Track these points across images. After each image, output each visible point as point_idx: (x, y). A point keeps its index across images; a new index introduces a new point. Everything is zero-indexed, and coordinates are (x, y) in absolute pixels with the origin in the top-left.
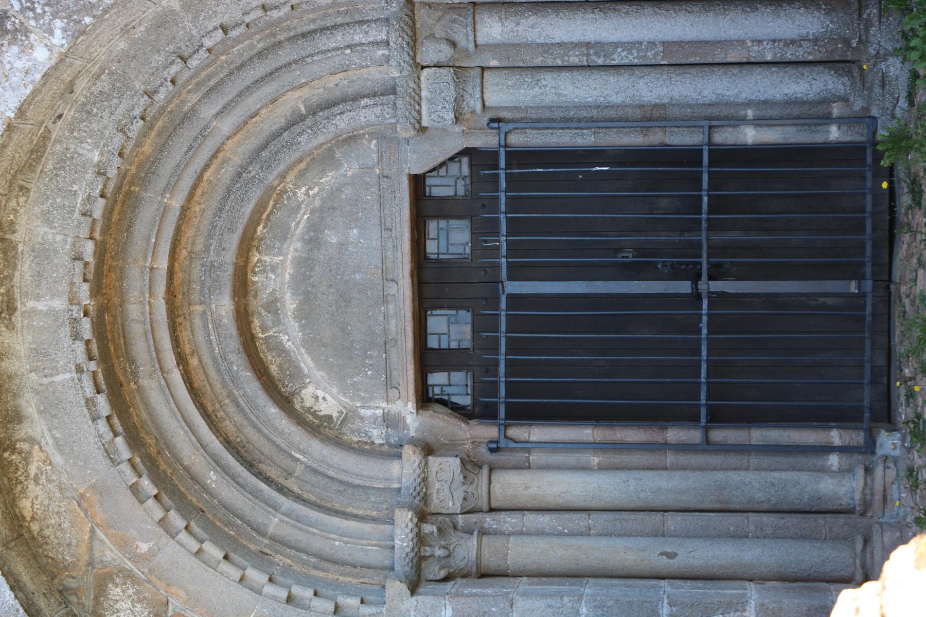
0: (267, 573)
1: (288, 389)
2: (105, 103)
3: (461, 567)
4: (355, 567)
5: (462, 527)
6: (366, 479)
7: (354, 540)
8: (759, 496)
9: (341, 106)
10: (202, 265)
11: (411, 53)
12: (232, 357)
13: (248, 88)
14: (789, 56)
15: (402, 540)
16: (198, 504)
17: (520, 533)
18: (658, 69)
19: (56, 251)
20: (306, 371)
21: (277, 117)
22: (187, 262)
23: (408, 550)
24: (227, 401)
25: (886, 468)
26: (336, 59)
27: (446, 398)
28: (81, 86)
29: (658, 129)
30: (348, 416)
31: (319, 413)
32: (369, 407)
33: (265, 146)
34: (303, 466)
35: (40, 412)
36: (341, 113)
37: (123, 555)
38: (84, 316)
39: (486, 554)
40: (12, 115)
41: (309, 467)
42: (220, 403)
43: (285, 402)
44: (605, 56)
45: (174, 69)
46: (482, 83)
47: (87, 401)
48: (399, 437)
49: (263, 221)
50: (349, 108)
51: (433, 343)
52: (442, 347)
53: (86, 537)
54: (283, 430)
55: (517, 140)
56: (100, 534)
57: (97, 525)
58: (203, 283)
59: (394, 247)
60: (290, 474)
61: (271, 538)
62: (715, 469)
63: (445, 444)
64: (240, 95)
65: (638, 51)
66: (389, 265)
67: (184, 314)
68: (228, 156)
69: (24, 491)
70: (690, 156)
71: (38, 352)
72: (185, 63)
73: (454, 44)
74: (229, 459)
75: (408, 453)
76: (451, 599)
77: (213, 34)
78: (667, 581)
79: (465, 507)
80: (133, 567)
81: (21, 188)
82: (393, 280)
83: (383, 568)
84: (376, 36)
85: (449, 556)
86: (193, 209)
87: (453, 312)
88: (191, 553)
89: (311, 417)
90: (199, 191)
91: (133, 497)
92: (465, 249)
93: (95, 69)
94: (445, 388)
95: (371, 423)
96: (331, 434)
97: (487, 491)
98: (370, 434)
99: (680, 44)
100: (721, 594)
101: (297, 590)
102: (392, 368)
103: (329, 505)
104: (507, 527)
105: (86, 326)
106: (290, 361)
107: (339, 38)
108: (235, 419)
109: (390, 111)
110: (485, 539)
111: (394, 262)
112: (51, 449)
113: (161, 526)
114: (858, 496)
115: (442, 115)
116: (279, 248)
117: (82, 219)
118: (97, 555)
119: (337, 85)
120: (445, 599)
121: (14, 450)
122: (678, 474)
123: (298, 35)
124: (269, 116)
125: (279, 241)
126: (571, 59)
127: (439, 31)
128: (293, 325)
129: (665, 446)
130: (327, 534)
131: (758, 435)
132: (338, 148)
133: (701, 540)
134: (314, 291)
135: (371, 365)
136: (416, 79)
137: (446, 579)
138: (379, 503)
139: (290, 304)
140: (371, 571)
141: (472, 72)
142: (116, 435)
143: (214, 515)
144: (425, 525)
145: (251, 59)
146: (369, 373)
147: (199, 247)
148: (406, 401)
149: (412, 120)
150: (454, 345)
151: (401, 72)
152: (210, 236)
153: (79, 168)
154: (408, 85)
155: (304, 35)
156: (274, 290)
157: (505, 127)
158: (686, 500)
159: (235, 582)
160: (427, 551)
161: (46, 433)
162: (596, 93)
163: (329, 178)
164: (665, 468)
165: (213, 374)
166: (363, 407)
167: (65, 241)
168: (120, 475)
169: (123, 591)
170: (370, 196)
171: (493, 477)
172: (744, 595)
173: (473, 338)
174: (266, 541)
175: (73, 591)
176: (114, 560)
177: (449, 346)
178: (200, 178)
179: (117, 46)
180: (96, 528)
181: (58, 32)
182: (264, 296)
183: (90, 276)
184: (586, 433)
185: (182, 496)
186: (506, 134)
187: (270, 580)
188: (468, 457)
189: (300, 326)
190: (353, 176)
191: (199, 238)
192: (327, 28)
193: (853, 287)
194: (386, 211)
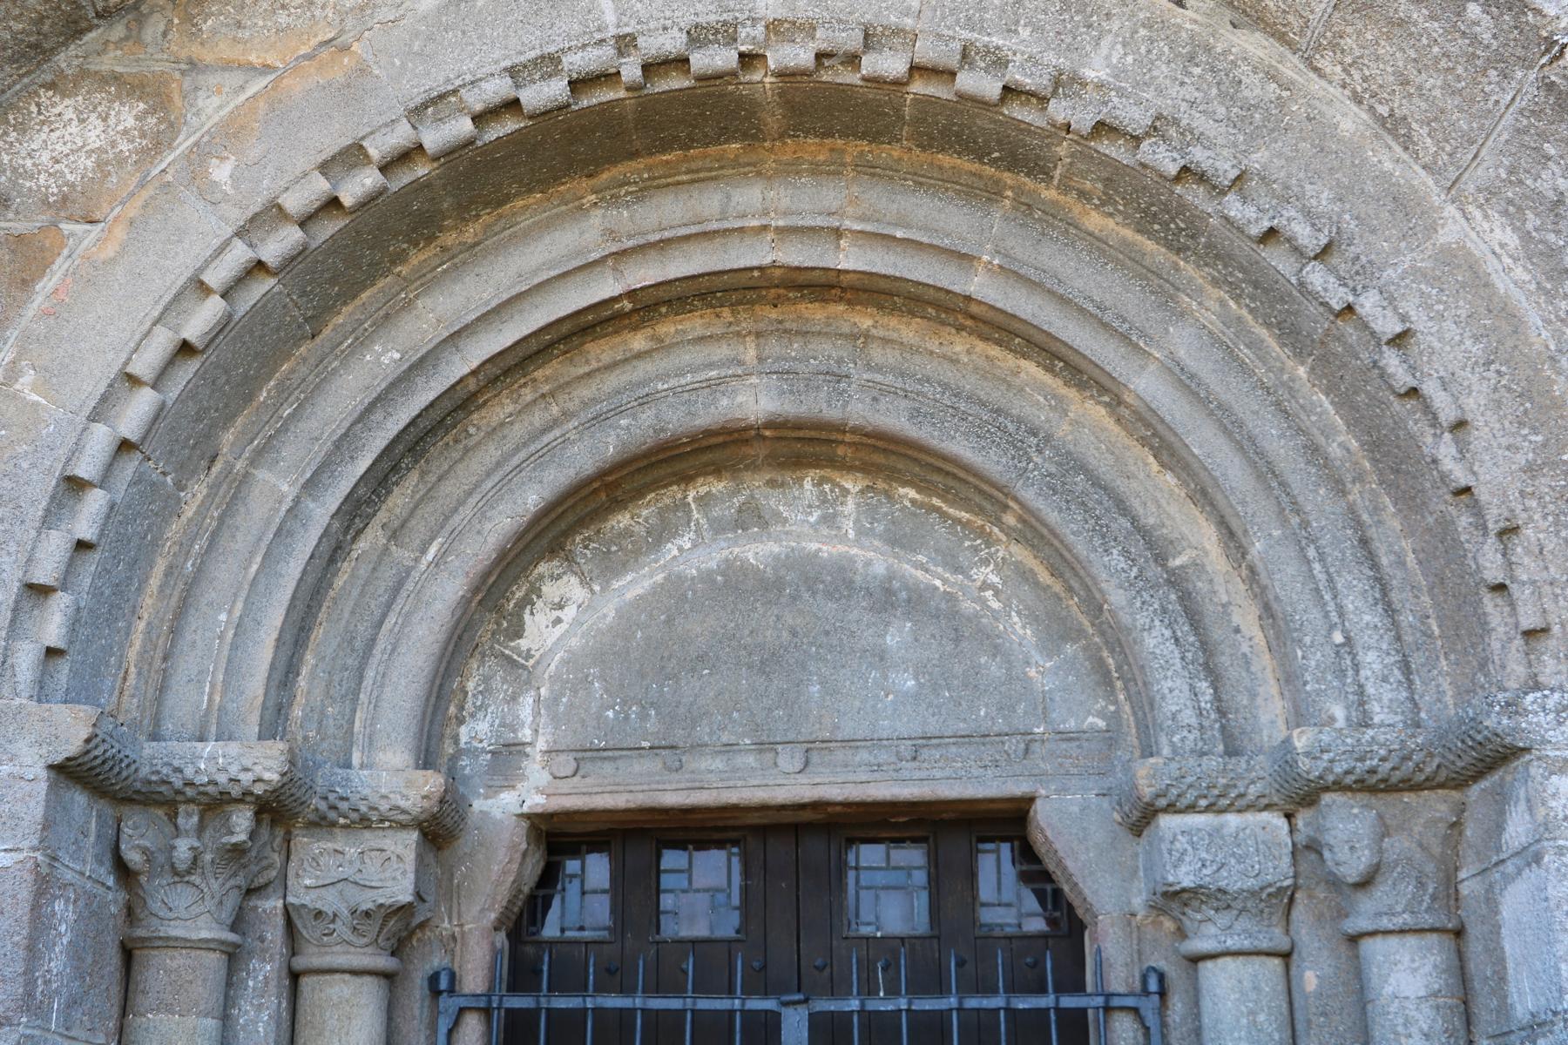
0: (144, 438)
1: (579, 549)
2: (1214, 91)
3: (150, 902)
4: (165, 659)
5: (256, 907)
6: (375, 693)
7: (226, 653)
9: (1192, 639)
10: (840, 361)
11: (1349, 780)
12: (647, 417)
15: (213, 758)
16: (330, 327)
20: (616, 584)
21: (1159, 506)
22: (846, 329)
23: (189, 772)
24: (555, 410)
26: (1315, 614)
30: (518, 670)
31: (527, 611)
33: (1096, 482)
34: (412, 564)
36: (1177, 640)
37: (208, 132)
38: (742, 55)
39: (176, 960)
41: (408, 574)
42: (552, 394)
46: (1258, 953)
48: (470, 777)
49: (926, 500)
50: (1189, 655)
52: (664, 877)
53: (253, 58)
54: (490, 519)
57: (280, 78)
59: (879, 765)
61: (247, 474)
63: (452, 875)
66: (840, 755)
67: (738, 323)
68: (1073, 408)
72: (1315, 258)
75: (426, 782)
76: (30, 865)
77: (1389, 312)
79: (301, 917)
80: (178, 152)
82: (807, 763)
83: (157, 720)
84: (1379, 700)
85: (176, 873)
86: (957, 339)
87: (736, 901)
88: (202, 269)
89: (519, 595)
91: (336, 149)
92: (869, 924)
94: (576, 883)
95: (503, 718)
96: (484, 633)
97: (335, 966)
98: (480, 715)
101: (95, 502)
102: (620, 763)
104: (247, 1012)
106: (637, 553)
107: (1367, 618)
108: (517, 426)
109: (1189, 744)
110: (214, 960)
111: (846, 766)
115: (1187, 859)
116: (872, 529)
117: (957, 46)
118: (212, 80)
119: (1237, 630)
120: (34, 849)
123: (1363, 532)
124: (1161, 490)
125: (887, 530)
127: (1398, 845)
128: (712, 557)
130: (244, 594)
132: (1085, 649)
134: (783, 600)
135: (627, 718)
136: (1265, 801)
137: (123, 871)
138: (320, 723)
139: (757, 551)
141: (1278, 931)
142: (479, 119)
143: (304, 360)
144: (249, 814)
145: (1300, 431)
146: (610, 714)
148: (551, 791)
149: (1175, 791)
150: (667, 901)
151: (1307, 754)
153: (1069, 40)
154: (1253, 782)
155: (1364, 542)
156: (786, 520)
157: (1149, 1006)
159: (126, 364)
160: (188, 819)
165: (613, 381)
166: (538, 700)
167: (907, 12)
168: (386, 125)
169: (125, 132)
170: (987, 714)
171: (368, 979)
173: (681, 941)
174: (239, 466)
175: (134, 33)
176: (197, 114)
177: (666, 871)
179: (1344, 115)
180: (271, 77)
182: (772, 501)
188: (422, 925)
189: (710, 573)
191: (897, 353)
192: (1385, 592)
194: (953, 749)
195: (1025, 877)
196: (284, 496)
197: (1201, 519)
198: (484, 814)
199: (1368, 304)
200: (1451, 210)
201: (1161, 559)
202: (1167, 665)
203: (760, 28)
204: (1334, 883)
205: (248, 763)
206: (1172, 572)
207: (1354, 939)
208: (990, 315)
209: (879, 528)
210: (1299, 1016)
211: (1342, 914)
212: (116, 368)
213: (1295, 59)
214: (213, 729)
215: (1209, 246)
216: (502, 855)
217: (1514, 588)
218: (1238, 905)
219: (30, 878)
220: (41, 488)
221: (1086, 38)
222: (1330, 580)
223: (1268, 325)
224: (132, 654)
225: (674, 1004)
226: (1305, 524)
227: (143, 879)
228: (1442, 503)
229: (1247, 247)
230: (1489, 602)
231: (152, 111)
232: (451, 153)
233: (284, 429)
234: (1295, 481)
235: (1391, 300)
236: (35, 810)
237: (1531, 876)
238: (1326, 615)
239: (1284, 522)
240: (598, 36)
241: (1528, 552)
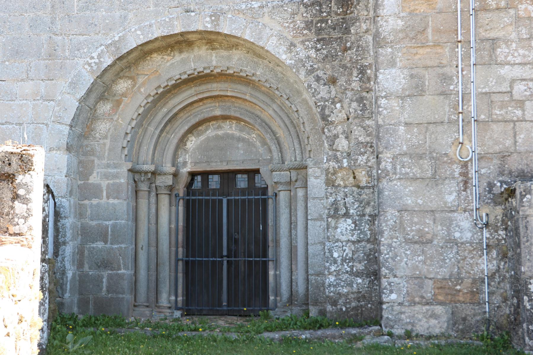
8: (161, 275)
12: (202, 115)
13: (282, 119)
14: (293, 283)
19: (230, 62)
25: (169, 313)
28: (279, 69)
30: (186, 151)
33: (266, 124)
43: (191, 131)
45: (285, 96)
47: (186, 72)
51: (210, 177)
55: (270, 201)
56: (146, 77)
58: (225, 106)
60: (167, 133)
61: (147, 128)
64: (280, 116)
69: (159, 54)
70: (265, 255)
71: (200, 58)
73: (296, 181)
74: (171, 115)
81: (249, 52)
83: (138, 162)
90: (252, 104)
93: (284, 73)
96: (181, 145)
99: (297, 251)
101: (130, 135)
105: (208, 71)
110: (147, 192)
112: (171, 62)
114: (161, 304)
118: (140, 76)
121: (171, 51)
122: (168, 251)
127: (299, 177)
128: (213, 134)
129: (177, 248)
131: (180, 275)
137: (135, 181)
139: (220, 133)
145: (291, 119)
147: (236, 105)
150: (210, 183)
152: (239, 108)
155: (298, 135)
157: (274, 198)
158: (160, 253)
160: (143, 175)
163: (258, 144)
164: (170, 247)
172: (129, 269)
178: (256, 104)
181: (291, 62)
182: (223, 125)
183: (223, 72)
184: (181, 224)
185: (159, 101)
187: (133, 128)
192: (300, 142)
193: (225, 304)
220: (123, 134)
224: (134, 153)
225: (209, 198)
233: (151, 121)
236: (126, 175)
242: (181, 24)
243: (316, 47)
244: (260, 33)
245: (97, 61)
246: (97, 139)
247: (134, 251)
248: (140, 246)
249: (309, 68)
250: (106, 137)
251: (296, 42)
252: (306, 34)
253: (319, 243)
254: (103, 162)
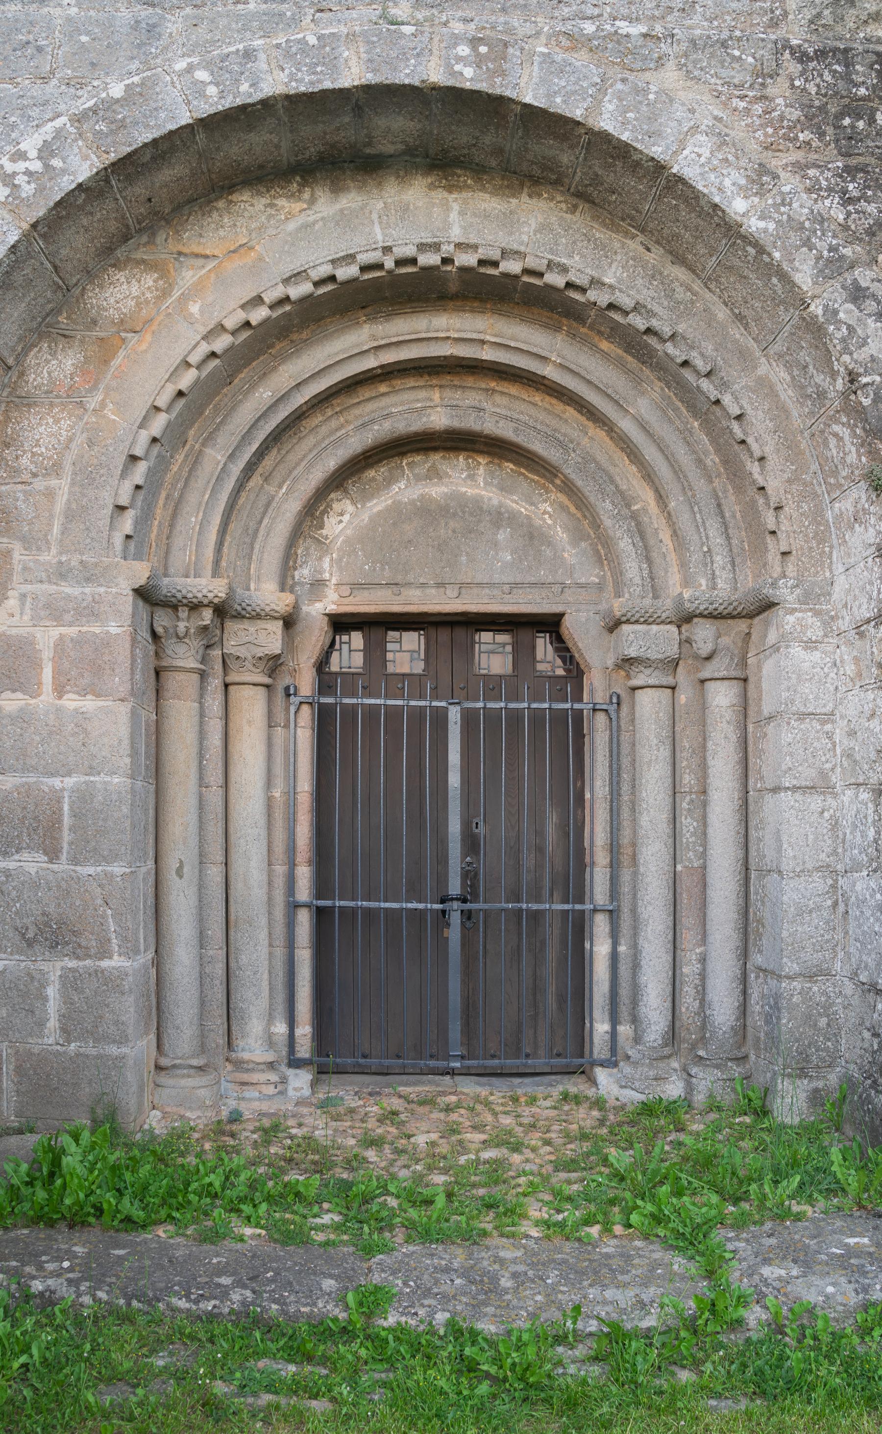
11: (706, 612)
17: (202, 715)
18: (672, 863)
19: (511, 234)
20: (368, 505)
26: (696, 537)
27: (337, 646)
29: (608, 860)
32: (331, 566)
35: (342, 210)
39: (181, 676)
40: (674, 171)
41: (273, 499)
44: (689, 809)
46: (662, 687)
56: (211, 265)
57: (221, 262)
61: (201, 451)
62: (270, 913)
65: (694, 843)
78: (154, 866)
83: (166, 568)
85: (178, 637)
87: (422, 656)
88: (187, 356)
91: (248, 298)
96: (305, 528)
100: (137, 929)
101: (142, 467)
103: (233, 518)
106: (378, 489)
109: (637, 592)
110: (196, 677)
112: (301, 220)
113: (216, 327)
119: (661, 541)
126: (687, 776)
127: (725, 641)
130: (203, 508)
132: (591, 545)
133: (197, 903)
135: (375, 570)
137: (154, 635)
139: (436, 491)
140: (162, 555)
142: (317, 284)
149: (630, 614)
150: (390, 656)
155: (719, 505)
158: (237, 887)
160: (183, 613)
161: (320, 215)
162: (651, 801)
164: (270, 864)
166: (332, 560)
167: (522, 243)
169: (149, 288)
171: (260, 688)
176: (182, 279)
181: (762, 224)
184: (305, 785)
186: (606, 711)
189: (414, 500)
190: (563, 557)
192: (726, 529)
195: (557, 650)
196: (219, 462)
197: (647, 488)
198: (308, 614)
199: (727, 399)
200: (763, 360)
201: (628, 506)
202: (629, 556)
203: (452, 246)
204: (696, 657)
205: (211, 588)
206: (633, 512)
207: (703, 681)
208: (553, 385)
209: (495, 482)
210: (677, 714)
211: (698, 670)
212: (149, 404)
213: (699, 282)
214: (193, 572)
215: (657, 363)
216: (317, 632)
217: (779, 533)
218: (655, 665)
219: (129, 638)
221: (605, 262)
222: (703, 522)
223: (683, 402)
224: (153, 536)
226: (694, 496)
227: (163, 640)
228: (752, 492)
229: (675, 367)
230: (769, 539)
231: (161, 278)
232: (303, 300)
233: (217, 429)
234: (690, 475)
235: (736, 398)
237: (776, 656)
238: (701, 538)
239: (685, 494)
240: (374, 246)
241: (786, 518)
242: (364, 56)
243: (844, 191)
244: (652, 118)
245: (36, 166)
246: (25, 477)
247: (151, 880)
248: (171, 863)
249: (825, 253)
250: (56, 469)
251: (776, 163)
252: (808, 143)
253: (818, 869)
254: (45, 557)
